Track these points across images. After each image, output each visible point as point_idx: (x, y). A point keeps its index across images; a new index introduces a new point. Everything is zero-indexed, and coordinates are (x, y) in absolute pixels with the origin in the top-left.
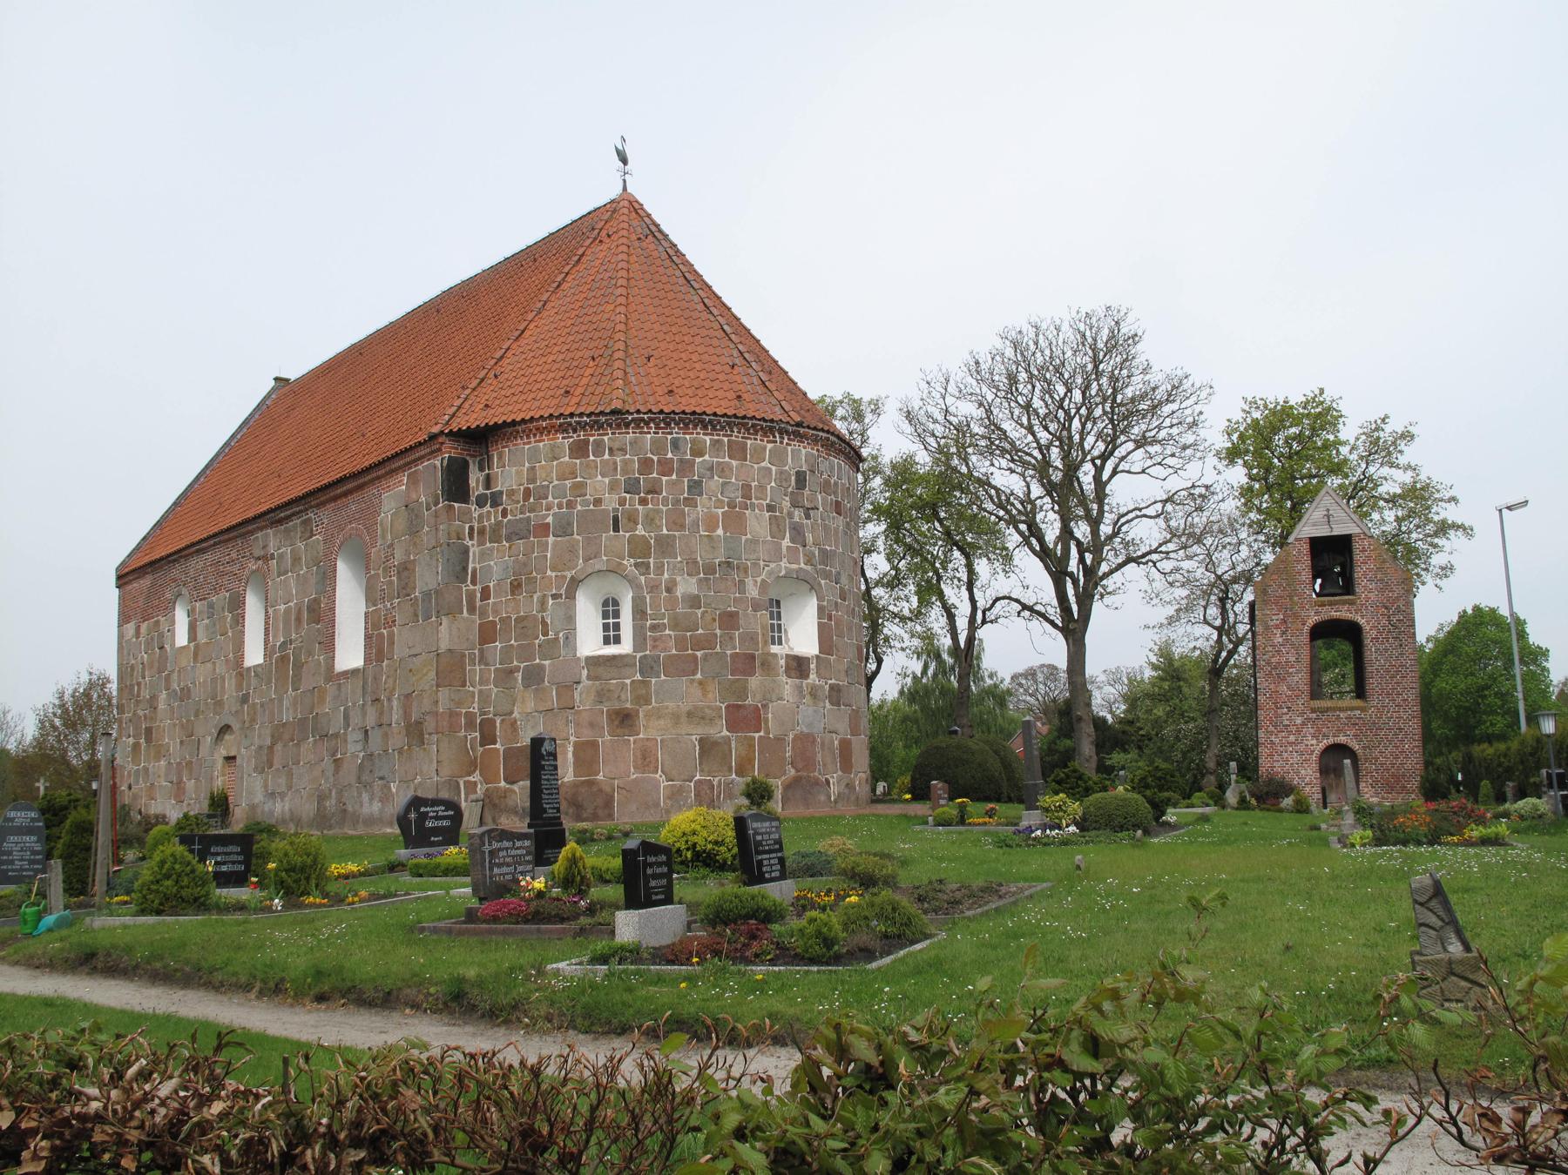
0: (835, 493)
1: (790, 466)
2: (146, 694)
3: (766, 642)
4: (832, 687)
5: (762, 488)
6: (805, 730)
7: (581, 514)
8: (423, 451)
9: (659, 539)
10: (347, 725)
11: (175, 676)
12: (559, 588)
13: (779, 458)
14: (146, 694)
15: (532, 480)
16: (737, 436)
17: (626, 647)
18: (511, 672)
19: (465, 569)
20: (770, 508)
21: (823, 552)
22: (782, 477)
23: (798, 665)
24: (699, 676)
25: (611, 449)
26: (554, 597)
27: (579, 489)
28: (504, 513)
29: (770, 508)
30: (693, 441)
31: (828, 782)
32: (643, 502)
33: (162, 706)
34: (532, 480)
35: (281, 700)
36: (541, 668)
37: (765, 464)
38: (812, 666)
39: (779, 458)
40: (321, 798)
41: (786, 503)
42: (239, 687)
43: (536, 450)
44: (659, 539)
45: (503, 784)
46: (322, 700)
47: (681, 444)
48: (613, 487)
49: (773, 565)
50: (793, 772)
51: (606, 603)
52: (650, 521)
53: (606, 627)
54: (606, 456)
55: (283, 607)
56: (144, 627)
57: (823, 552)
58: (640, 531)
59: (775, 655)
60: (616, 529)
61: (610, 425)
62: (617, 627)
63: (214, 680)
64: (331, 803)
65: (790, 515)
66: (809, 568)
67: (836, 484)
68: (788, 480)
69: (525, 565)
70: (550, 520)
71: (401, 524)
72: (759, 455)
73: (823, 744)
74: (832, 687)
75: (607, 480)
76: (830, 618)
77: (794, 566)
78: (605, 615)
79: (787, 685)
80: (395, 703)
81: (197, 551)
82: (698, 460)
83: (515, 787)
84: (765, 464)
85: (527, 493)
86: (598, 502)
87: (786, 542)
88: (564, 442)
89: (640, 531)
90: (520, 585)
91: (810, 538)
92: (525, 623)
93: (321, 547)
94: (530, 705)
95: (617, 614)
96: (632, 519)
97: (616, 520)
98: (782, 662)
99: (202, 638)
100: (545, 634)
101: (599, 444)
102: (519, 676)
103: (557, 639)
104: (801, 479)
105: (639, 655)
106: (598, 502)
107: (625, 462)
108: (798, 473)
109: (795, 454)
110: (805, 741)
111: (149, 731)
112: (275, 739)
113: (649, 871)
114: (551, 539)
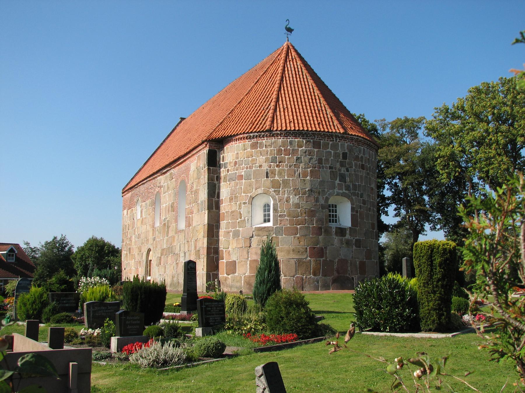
0: (362, 161)
1: (340, 151)
2: (129, 236)
3: (327, 222)
4: (356, 240)
5: (327, 160)
6: (343, 258)
7: (255, 171)
8: (201, 147)
9: (284, 181)
10: (180, 250)
11: (136, 230)
12: (246, 200)
13: (335, 147)
14: (129, 236)
15: (237, 158)
16: (316, 139)
17: (270, 224)
18: (229, 232)
19: (215, 193)
20: (331, 168)
21: (354, 186)
22: (336, 155)
23: (341, 231)
24: (298, 235)
25: (265, 145)
26: (244, 203)
27: (254, 161)
28: (228, 171)
29: (331, 168)
30: (298, 142)
31: (353, 278)
32: (277, 166)
33: (133, 241)
34: (237, 158)
35: (163, 239)
36: (239, 231)
37: (329, 150)
38: (348, 232)
39: (335, 147)
40: (173, 277)
41: (338, 165)
42: (153, 235)
43: (238, 146)
44: (284, 181)
45: (225, 275)
46: (174, 240)
47: (293, 143)
48: (267, 160)
49: (331, 191)
50: (337, 275)
51: (265, 206)
52: (280, 174)
53: (265, 216)
54: (264, 148)
55: (164, 205)
56: (129, 211)
57: (354, 186)
58: (277, 178)
59: (331, 227)
60: (267, 177)
61: (267, 136)
62: (269, 215)
63: (147, 232)
64: (175, 279)
65: (340, 170)
66: (347, 192)
67: (362, 157)
68: (339, 156)
69: (234, 191)
70: (243, 173)
71: (195, 176)
72: (326, 146)
73: (351, 263)
74: (356, 240)
75: (264, 158)
76: (357, 212)
77: (341, 191)
78: (265, 211)
79: (336, 240)
80: (193, 243)
81: (142, 184)
82: (300, 149)
83: (229, 276)
84: (329, 150)
85: (236, 163)
86: (260, 166)
87: (337, 182)
88: (248, 143)
89: (277, 178)
90: (232, 199)
91: (348, 179)
92: (233, 214)
93: (174, 183)
94: (235, 245)
95: (269, 210)
96: (273, 173)
97: (267, 173)
98: (334, 230)
99: (144, 216)
100: (241, 218)
101: (261, 143)
102: (231, 234)
103: (245, 220)
104: (345, 156)
105: (275, 227)
106: (260, 166)
107: (271, 151)
108: (343, 153)
109: (342, 146)
110: (343, 262)
111: (130, 249)
112: (162, 254)
113: (127, 322)
114: (244, 181)
